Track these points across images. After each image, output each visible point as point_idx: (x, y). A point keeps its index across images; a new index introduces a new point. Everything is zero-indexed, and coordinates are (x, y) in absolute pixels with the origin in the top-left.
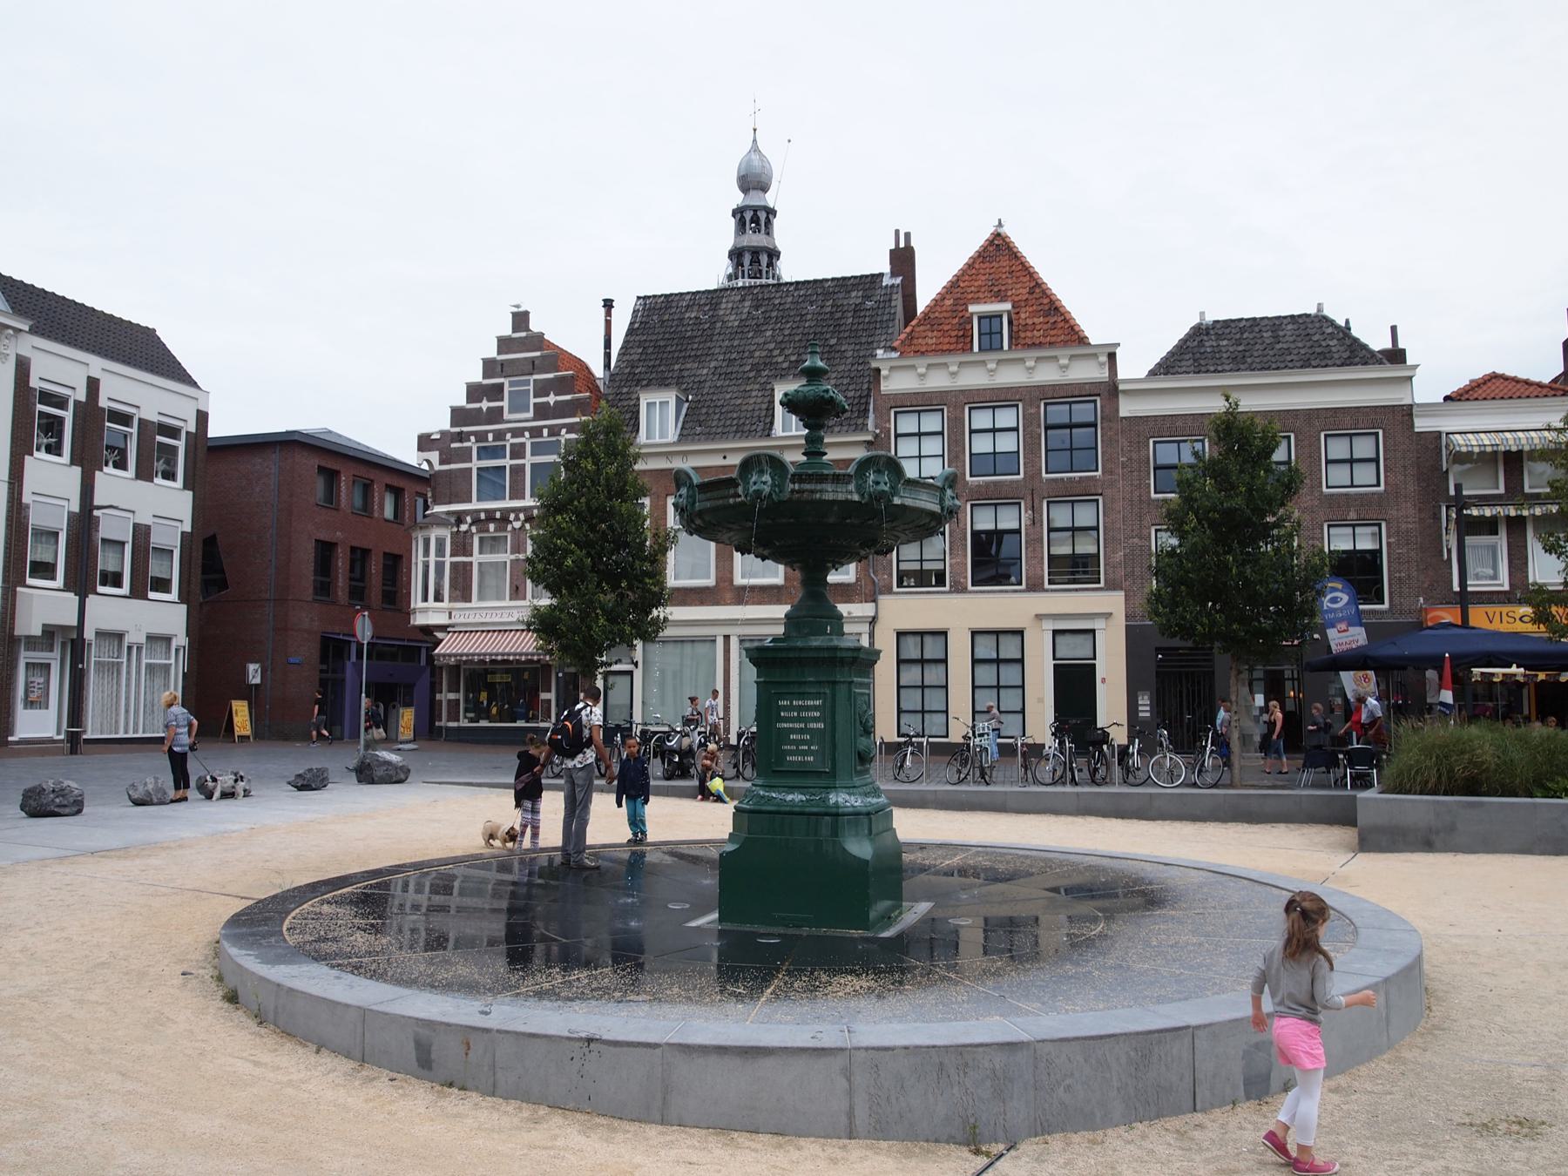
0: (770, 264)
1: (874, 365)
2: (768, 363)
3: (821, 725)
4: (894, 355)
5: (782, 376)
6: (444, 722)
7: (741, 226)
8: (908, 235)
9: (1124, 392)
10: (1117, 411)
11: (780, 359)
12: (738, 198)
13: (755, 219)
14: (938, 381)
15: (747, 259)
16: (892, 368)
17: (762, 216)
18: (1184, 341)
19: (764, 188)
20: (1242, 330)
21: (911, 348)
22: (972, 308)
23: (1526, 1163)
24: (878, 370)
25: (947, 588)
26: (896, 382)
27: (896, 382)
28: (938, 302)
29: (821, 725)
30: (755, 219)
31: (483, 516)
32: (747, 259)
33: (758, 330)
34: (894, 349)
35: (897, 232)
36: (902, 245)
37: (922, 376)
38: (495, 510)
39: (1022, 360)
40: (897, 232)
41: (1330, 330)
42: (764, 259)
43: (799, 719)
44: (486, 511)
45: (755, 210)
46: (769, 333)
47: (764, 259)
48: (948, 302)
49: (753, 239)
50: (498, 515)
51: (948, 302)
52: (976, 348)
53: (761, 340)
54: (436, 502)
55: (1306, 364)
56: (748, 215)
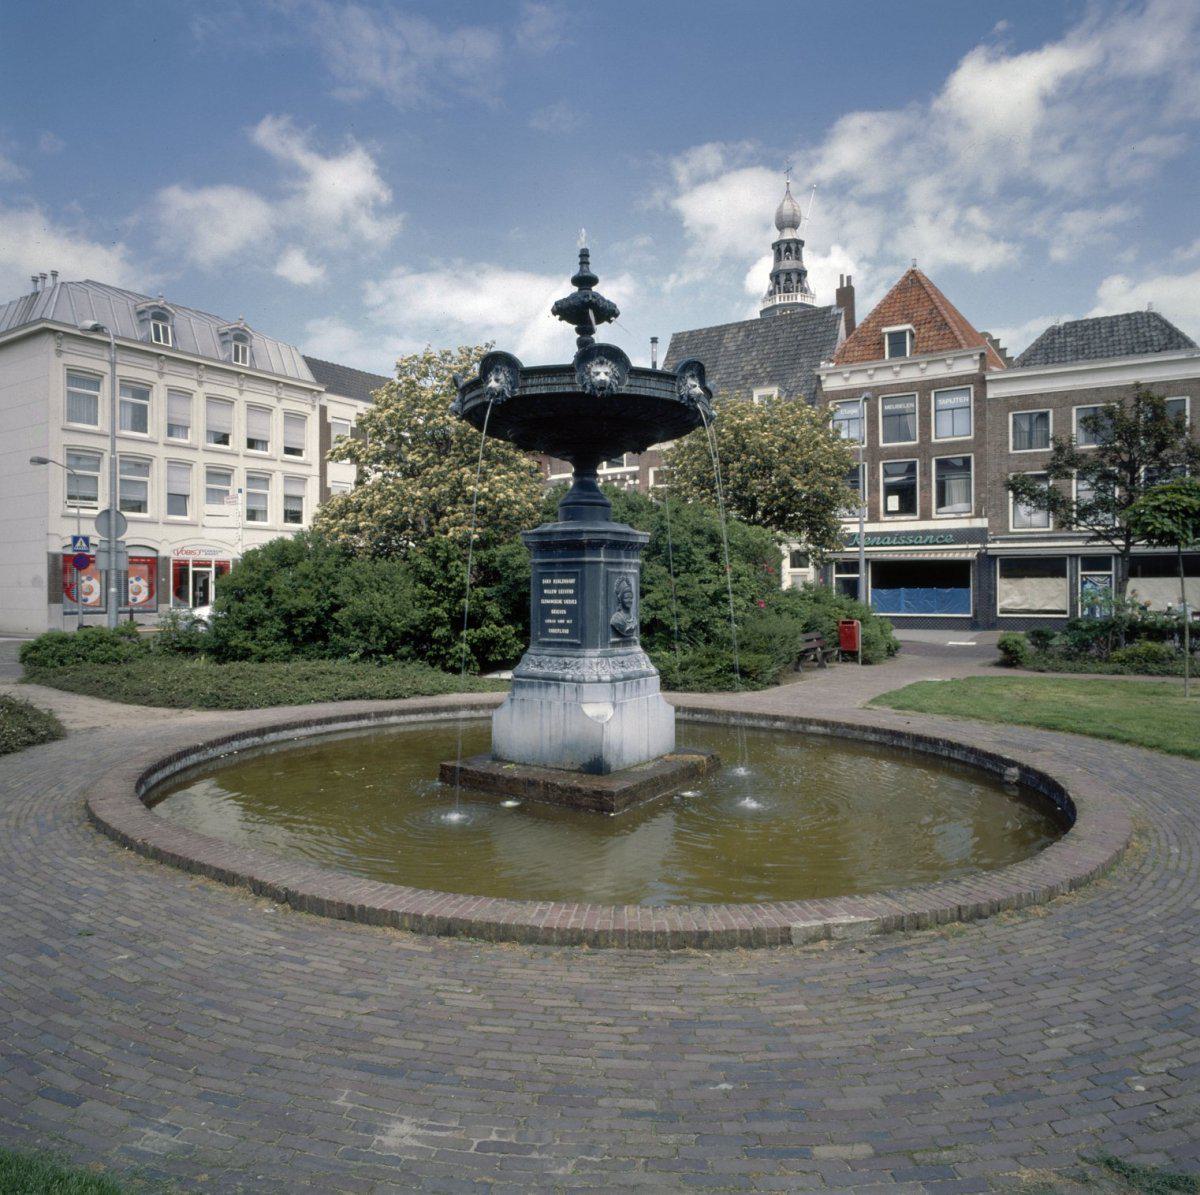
0: (799, 281)
1: (817, 373)
2: (753, 374)
3: (573, 602)
4: (832, 365)
5: (759, 383)
6: (145, 568)
7: (778, 258)
8: (849, 278)
9: (991, 381)
10: (985, 394)
11: (760, 371)
12: (775, 236)
13: (788, 249)
14: (859, 381)
15: (783, 279)
16: (828, 375)
17: (793, 246)
18: (1041, 340)
19: (794, 225)
20: (1086, 329)
21: (844, 358)
22: (885, 330)
23: (109, 552)
24: (819, 377)
25: (917, 517)
26: (831, 384)
27: (831, 384)
28: (868, 321)
29: (573, 602)
30: (788, 249)
31: (610, 478)
32: (783, 279)
33: (748, 352)
34: (831, 361)
35: (842, 276)
36: (845, 285)
37: (847, 379)
38: (616, 474)
39: (917, 364)
40: (842, 276)
41: (1157, 323)
42: (794, 277)
43: (557, 596)
44: (612, 475)
45: (788, 242)
46: (754, 354)
47: (794, 277)
48: (871, 325)
49: (788, 264)
50: (619, 477)
51: (871, 325)
52: (887, 357)
53: (749, 358)
54: (553, 473)
55: (1131, 351)
56: (783, 247)
